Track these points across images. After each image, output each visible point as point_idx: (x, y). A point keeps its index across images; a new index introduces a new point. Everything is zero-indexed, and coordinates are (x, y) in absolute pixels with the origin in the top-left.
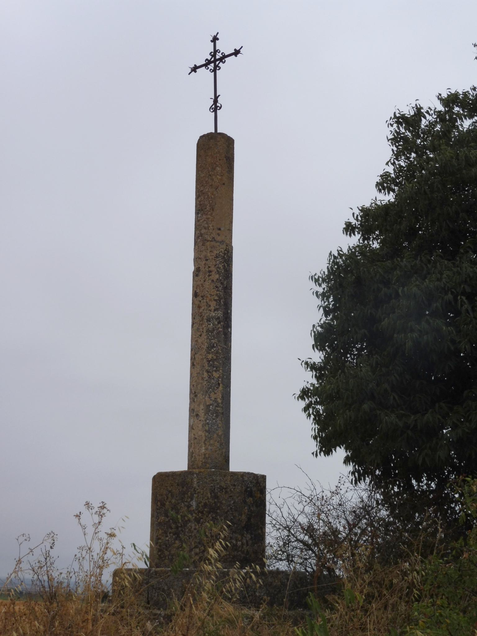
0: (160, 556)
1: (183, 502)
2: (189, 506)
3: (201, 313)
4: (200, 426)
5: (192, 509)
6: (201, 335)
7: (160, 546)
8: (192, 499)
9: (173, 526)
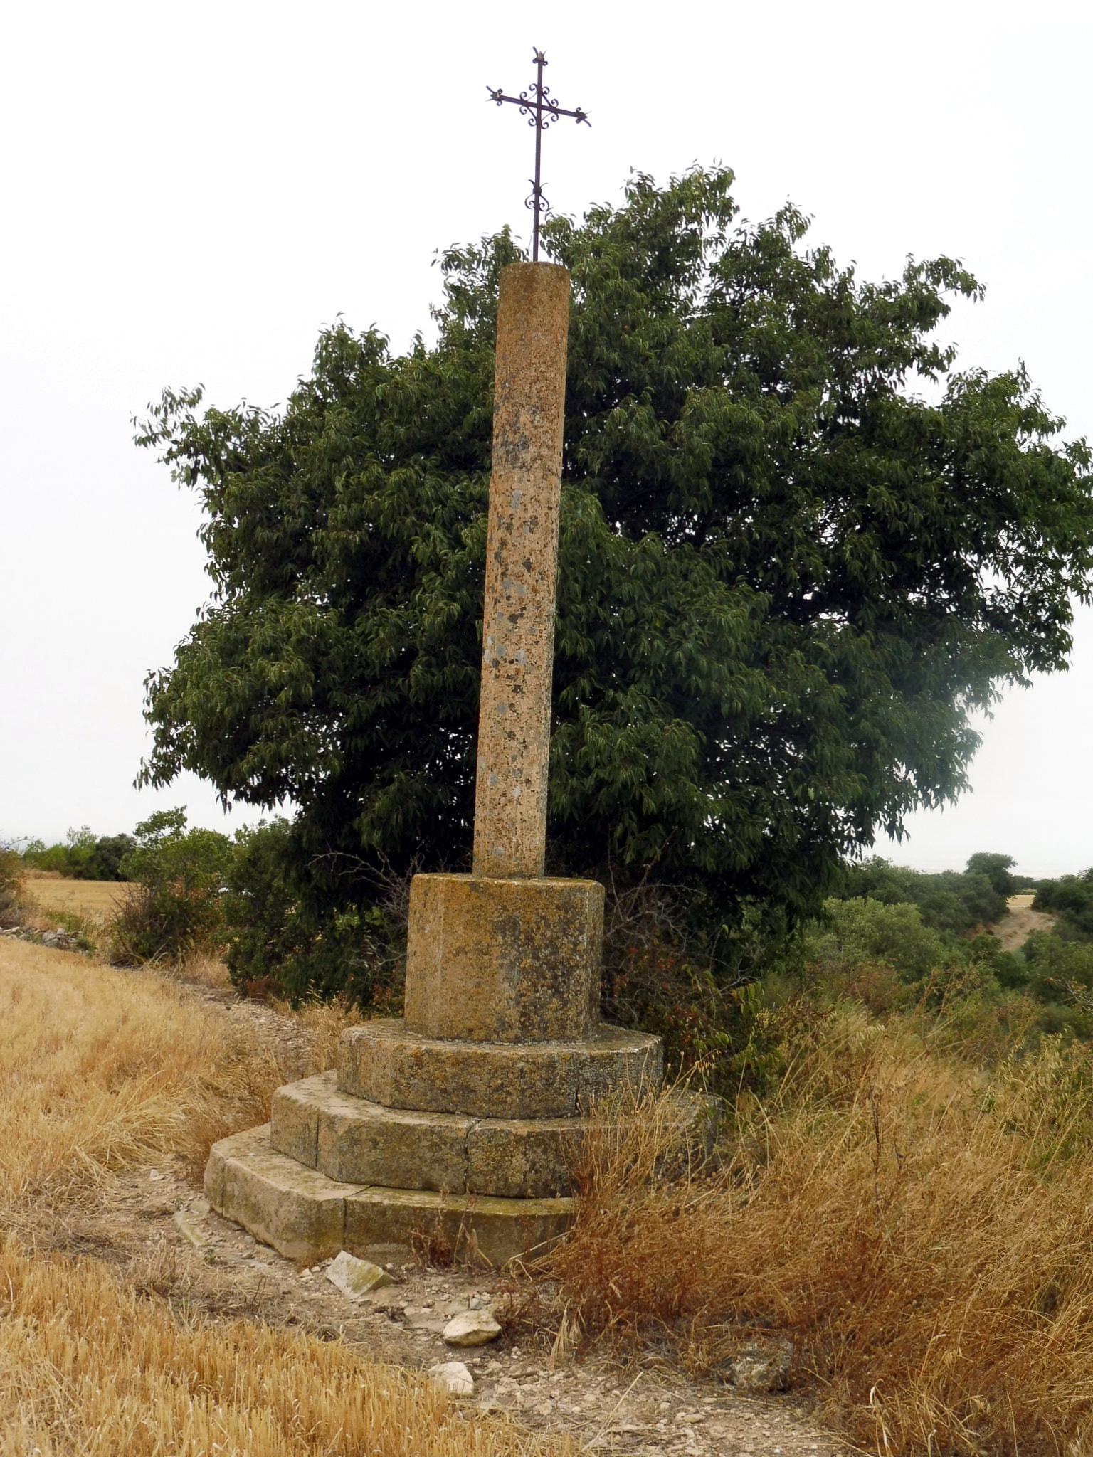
0: (522, 1023)
1: (566, 935)
2: (576, 944)
3: (538, 602)
4: (533, 800)
5: (582, 947)
6: (537, 643)
7: (524, 1007)
8: (582, 932)
9: (549, 974)
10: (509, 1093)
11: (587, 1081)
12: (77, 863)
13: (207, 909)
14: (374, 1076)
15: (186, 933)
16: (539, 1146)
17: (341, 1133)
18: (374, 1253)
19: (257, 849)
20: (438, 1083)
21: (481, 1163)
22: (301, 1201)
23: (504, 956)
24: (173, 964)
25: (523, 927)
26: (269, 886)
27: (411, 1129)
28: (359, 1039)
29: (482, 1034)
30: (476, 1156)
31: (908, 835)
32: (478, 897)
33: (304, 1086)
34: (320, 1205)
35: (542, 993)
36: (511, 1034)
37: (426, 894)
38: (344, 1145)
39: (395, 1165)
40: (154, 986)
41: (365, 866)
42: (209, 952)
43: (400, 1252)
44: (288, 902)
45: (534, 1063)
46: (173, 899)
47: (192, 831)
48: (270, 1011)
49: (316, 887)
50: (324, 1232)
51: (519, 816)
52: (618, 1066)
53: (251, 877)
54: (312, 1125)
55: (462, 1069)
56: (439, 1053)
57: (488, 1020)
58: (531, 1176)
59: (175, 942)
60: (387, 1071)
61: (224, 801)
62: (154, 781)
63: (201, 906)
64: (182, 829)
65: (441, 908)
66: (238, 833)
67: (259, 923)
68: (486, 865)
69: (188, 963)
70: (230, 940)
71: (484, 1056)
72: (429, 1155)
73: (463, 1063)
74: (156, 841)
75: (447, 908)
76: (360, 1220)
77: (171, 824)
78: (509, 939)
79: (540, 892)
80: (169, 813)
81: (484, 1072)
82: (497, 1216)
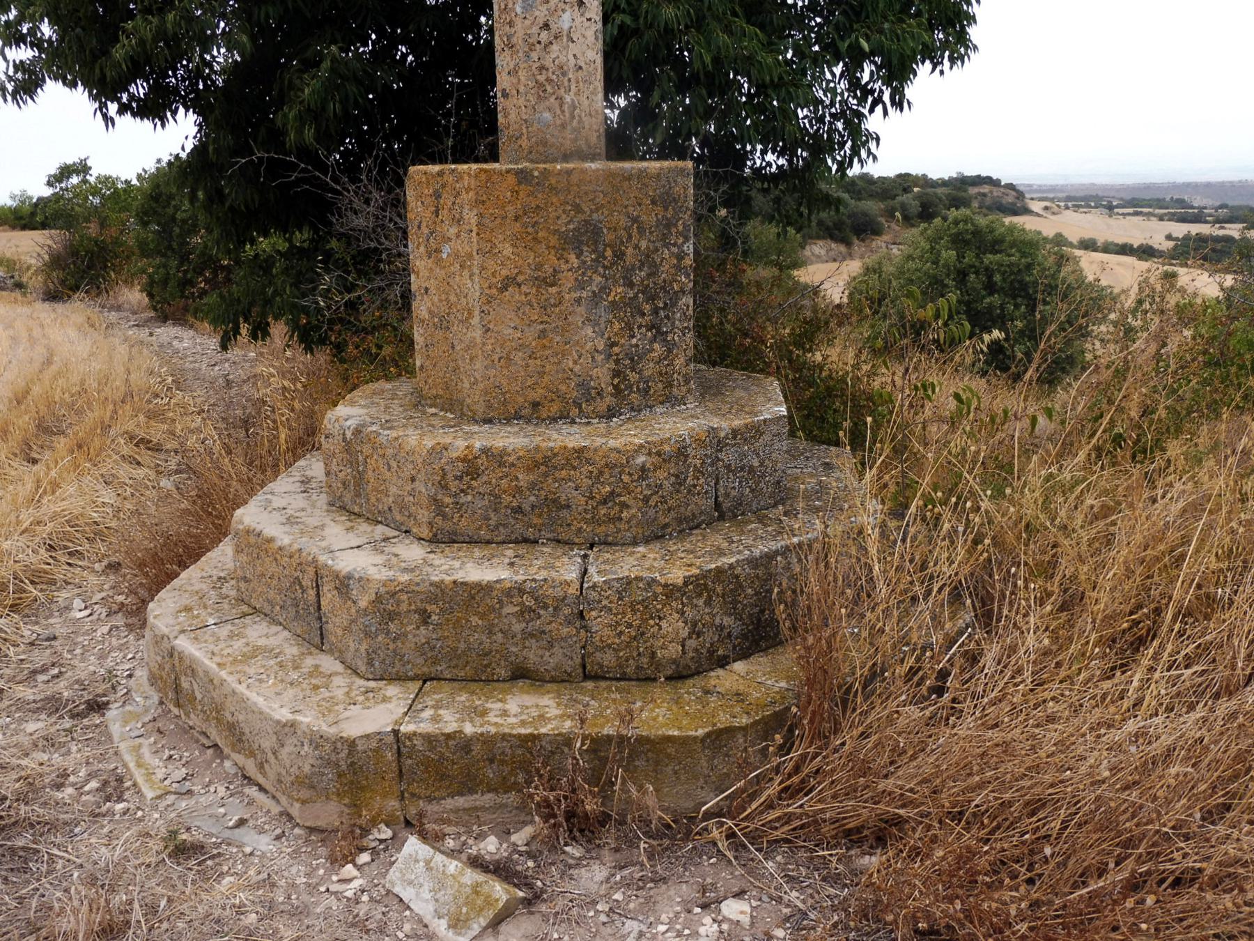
0: (616, 387)
1: (667, 245)
7: (617, 362)
9: (647, 308)
10: (624, 506)
11: (728, 467)
12: (21, 218)
13: (122, 245)
14: (393, 490)
15: (106, 266)
16: (700, 595)
17: (363, 603)
18: (457, 811)
19: (158, 186)
20: (507, 499)
21: (607, 632)
22: (317, 741)
23: (581, 286)
24: (98, 295)
25: (608, 237)
26: (174, 219)
27: (484, 589)
28: (357, 432)
29: (555, 408)
30: (599, 623)
31: (909, 103)
32: (531, 194)
33: (278, 502)
34: (352, 744)
35: (640, 338)
36: (602, 406)
37: (437, 195)
38: (373, 622)
39: (462, 646)
40: (79, 318)
41: (304, 170)
42: (129, 283)
43: (503, 806)
44: (193, 230)
45: (659, 454)
46: (89, 239)
47: (97, 178)
48: (191, 332)
49: (231, 208)
50: (369, 795)
51: (572, 61)
52: (767, 437)
53: (155, 212)
54: (307, 582)
55: (545, 475)
56: (504, 452)
57: (563, 388)
58: (692, 643)
59: (98, 276)
60: (420, 486)
61: (105, 116)
62: (14, 98)
63: (116, 242)
64: (88, 177)
65: (471, 217)
66: (139, 177)
67: (169, 253)
68: (524, 143)
69: (111, 293)
70: (144, 271)
71: (580, 451)
72: (517, 627)
73: (545, 464)
74: (67, 189)
75: (481, 215)
76: (427, 763)
77: (77, 172)
78: (589, 257)
79: (629, 179)
80: (74, 164)
81: (582, 476)
82: (669, 739)
